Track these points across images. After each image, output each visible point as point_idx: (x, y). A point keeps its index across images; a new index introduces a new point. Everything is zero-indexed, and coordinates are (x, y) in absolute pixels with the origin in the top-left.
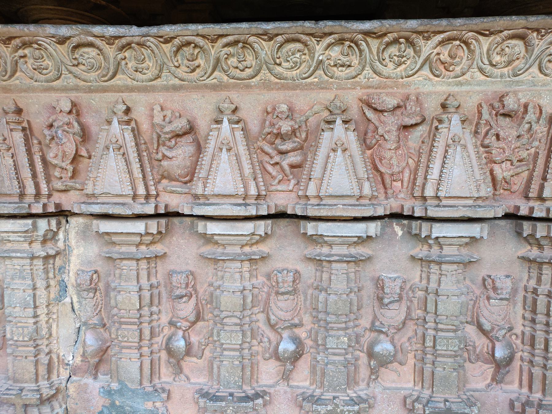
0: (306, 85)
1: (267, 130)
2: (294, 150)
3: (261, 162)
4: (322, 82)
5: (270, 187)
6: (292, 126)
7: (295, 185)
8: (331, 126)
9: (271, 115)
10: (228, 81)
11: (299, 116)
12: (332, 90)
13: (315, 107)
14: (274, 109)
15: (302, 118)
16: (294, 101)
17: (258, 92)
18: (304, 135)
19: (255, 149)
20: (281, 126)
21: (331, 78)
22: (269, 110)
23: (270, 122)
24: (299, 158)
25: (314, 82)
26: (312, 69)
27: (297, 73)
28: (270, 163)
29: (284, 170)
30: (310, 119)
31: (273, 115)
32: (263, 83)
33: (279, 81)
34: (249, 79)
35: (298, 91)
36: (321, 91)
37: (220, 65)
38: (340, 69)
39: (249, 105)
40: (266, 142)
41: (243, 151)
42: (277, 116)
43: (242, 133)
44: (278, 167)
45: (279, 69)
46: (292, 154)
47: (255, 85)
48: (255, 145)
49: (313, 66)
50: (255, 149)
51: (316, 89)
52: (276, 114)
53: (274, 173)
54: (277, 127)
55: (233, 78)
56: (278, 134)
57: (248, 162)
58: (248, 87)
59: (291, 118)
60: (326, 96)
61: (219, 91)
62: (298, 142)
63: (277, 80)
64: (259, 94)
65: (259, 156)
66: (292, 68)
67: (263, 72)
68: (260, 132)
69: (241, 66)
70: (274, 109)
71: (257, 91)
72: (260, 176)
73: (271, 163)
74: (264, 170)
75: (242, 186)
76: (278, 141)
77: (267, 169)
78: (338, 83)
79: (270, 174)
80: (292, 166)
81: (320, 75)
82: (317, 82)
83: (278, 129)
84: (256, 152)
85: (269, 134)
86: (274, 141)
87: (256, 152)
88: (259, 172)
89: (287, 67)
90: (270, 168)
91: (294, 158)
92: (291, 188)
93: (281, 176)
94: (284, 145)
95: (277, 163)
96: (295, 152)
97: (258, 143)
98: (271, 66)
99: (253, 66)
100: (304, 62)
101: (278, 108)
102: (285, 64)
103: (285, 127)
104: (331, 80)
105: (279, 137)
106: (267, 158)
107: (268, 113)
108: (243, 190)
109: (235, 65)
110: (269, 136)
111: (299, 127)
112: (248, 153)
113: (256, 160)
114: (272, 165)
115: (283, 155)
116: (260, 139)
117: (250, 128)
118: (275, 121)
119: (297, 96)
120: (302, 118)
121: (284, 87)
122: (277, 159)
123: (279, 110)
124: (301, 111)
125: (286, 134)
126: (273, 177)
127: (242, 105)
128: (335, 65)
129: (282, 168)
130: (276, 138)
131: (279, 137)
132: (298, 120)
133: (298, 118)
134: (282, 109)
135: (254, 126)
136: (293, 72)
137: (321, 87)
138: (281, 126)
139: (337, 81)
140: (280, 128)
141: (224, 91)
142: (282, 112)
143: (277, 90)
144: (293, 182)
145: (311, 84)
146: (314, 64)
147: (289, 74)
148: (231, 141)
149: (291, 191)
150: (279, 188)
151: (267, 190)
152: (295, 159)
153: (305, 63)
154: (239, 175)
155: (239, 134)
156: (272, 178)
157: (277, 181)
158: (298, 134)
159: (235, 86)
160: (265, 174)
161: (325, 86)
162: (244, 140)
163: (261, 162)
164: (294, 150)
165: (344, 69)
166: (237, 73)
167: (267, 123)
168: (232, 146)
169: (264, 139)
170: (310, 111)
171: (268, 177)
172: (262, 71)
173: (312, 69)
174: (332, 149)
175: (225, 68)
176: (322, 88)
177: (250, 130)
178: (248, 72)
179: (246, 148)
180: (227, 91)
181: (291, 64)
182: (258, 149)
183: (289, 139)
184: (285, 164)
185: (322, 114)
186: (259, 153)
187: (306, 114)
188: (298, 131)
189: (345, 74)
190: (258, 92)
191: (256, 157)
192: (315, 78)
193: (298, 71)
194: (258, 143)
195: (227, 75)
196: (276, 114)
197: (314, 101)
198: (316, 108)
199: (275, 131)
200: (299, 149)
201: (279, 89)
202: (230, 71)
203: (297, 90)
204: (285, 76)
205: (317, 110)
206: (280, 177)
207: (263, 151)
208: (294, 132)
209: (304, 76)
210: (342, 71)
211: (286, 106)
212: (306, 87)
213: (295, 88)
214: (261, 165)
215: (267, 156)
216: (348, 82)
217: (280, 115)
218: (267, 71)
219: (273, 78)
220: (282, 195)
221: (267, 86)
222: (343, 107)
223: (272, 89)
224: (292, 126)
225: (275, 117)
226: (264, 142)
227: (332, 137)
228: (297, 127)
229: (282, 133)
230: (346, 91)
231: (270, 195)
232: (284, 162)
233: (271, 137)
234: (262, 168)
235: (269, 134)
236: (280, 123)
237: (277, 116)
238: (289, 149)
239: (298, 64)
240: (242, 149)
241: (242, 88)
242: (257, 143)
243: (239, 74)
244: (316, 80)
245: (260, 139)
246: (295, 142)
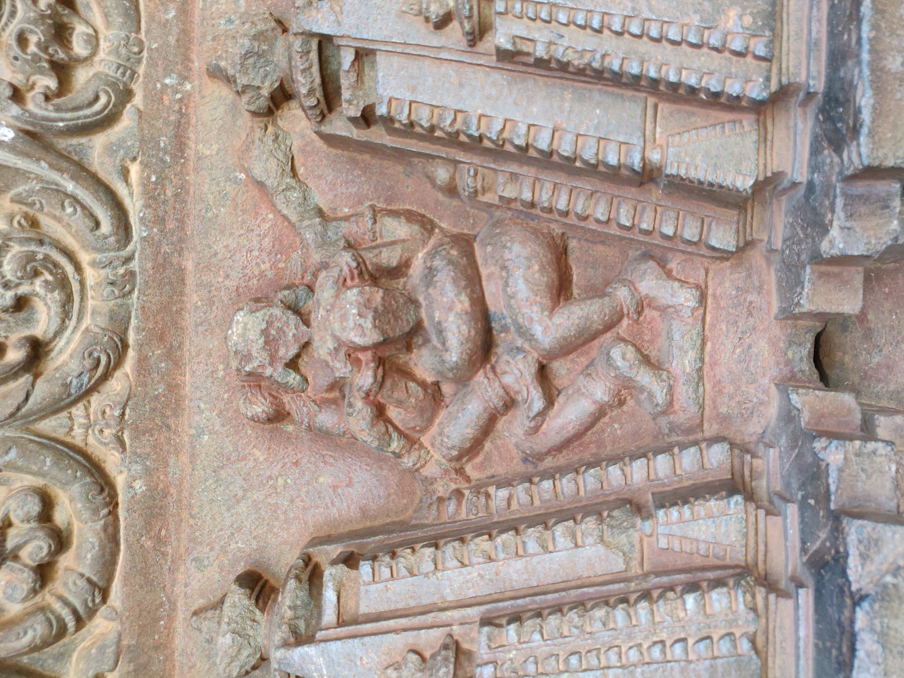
0: (160, 221)
1: (358, 421)
2: (472, 280)
3: (536, 466)
4: (147, 141)
5: (680, 418)
6: (342, 284)
7: (669, 274)
8: (347, 58)
9: (286, 398)
10: (116, 615)
11: (296, 256)
12: (189, 95)
13: (258, 171)
14: (255, 380)
15: (309, 236)
16: (231, 284)
17: (184, 458)
18: (398, 229)
19: (459, 493)
20: (340, 344)
21: (127, 95)
22: (260, 407)
23: (322, 404)
24: (517, 248)
25: (145, 183)
26: (70, 186)
27: (93, 264)
28: (542, 414)
29: (581, 332)
30: (319, 199)
31: (287, 388)
32: (138, 433)
33: (131, 353)
34: (112, 503)
35: (189, 265)
36: (190, 153)
37: (25, 660)
38: (79, 48)
39: (242, 508)
40: (424, 430)
41: (472, 573)
42: (293, 364)
43: (365, 568)
44: (560, 368)
45: (66, 358)
46: (491, 290)
47: (148, 472)
48: (441, 489)
49: (55, 176)
50: (459, 493)
51: (181, 174)
52: (277, 372)
53: (599, 390)
54: (341, 369)
55: (101, 590)
56: (381, 362)
57: (532, 546)
58: (154, 508)
59: (302, 292)
60: (216, 119)
61: (169, 658)
62: (432, 255)
63: (129, 365)
64: (193, 456)
65: (500, 470)
66: (63, 283)
67: (78, 431)
68: (378, 457)
69: (36, 548)
70: (255, 380)
71: (178, 464)
72: (614, 471)
73: (538, 404)
74: (581, 449)
75: (690, 600)
76: (423, 364)
77: (571, 430)
78: (152, 63)
79: (600, 413)
80: (561, 289)
81: (111, 150)
82: (145, 165)
83: (357, 363)
84: (479, 489)
85: (380, 412)
86: (423, 384)
87: (479, 489)
88: (590, 480)
89: (55, 309)
90: (570, 414)
91: (516, 279)
92: (685, 298)
93: (616, 353)
94: (440, 332)
95: (543, 373)
96: (484, 272)
97: (431, 470)
98: (43, 390)
99: (39, 482)
100: (34, 224)
101: (248, 357)
102: (43, 321)
103: (346, 319)
104: (138, 100)
105: (403, 358)
106: (513, 430)
107: (278, 416)
108: (718, 599)
109: (25, 580)
110: (393, 413)
111: (349, 246)
112: (483, 543)
113: (520, 491)
114: (550, 401)
115: (501, 338)
116: (408, 461)
117: (354, 512)
118: (319, 380)
119: (208, 267)
120: (309, 236)
121: (166, 330)
122: (515, 371)
123: (259, 358)
124: (281, 248)
125: (383, 315)
126: (624, 392)
127: (241, 551)
128: (62, 71)
129: (569, 347)
130: (408, 375)
131: (403, 358)
132: (316, 257)
133: (306, 257)
134: (254, 334)
135: (346, 490)
136: (90, 281)
137: (170, 151)
138: (340, 344)
139: (141, 70)
140: (352, 353)
141: (170, 630)
142: (270, 342)
143: (177, 364)
144: (649, 283)
145: (151, 196)
146: (42, 169)
147: (96, 303)
148: (410, 638)
149: (702, 299)
150: (683, 363)
151: (692, 436)
152: (519, 273)
153: (45, 221)
154: (619, 614)
155: (376, 587)
156: (622, 403)
157: (645, 377)
158: (390, 257)
159: (147, 577)
160: (600, 444)
161: (170, 131)
162: (406, 557)
163: (536, 466)
164: (472, 280)
165: (80, 30)
166: (76, 563)
167: (326, 419)
168: (436, 636)
169: (411, 441)
170: (279, 201)
171: (615, 429)
172: (78, 437)
173: (70, 186)
174: (473, 43)
175: (36, 630)
176: (180, 144)
177: (364, 511)
178: (70, 509)
179: (450, 549)
180: (171, 618)
181: (38, 286)
182: (460, 471)
183: (415, 303)
184: (549, 327)
185: (296, 144)
186: (481, 467)
187: (294, 218)
188: (369, 256)
189: (108, 24)
190: (184, 458)
191: (503, 493)
192: (125, 173)
193: (84, 258)
194: (431, 470)
195: (80, 622)
196: (277, 372)
197: (236, 181)
198: (267, 168)
199: (366, 378)
200: (470, 255)
201: (173, 357)
202: (57, 606)
203: (182, 270)
204: (102, 321)
205: (273, 164)
206: (622, 357)
207: (473, 448)
208: (375, 275)
209: (106, 227)
210: (94, 41)
211: (240, 317)
212: (171, 225)
213: (169, 279)
214: (549, 462)
215: (500, 425)
216: (151, 18)
217: (288, 352)
218: (78, 411)
219: (117, 385)
220: (725, 350)
221: (154, 418)
222: (261, 26)
223: (173, 388)
224: (342, 284)
225: (293, 378)
226: (425, 440)
227: (408, 52)
228: (346, 260)
229: (372, 337)
230: (197, 33)
231: (725, 419)
232: (538, 330)
233: (399, 403)
234: (562, 460)
235: (380, 412)
236: (323, 347)
237: (293, 364)
238: (463, 303)
239: (41, 252)
240: (459, 576)
241: (160, 541)
242: (429, 481)
243: (79, 558)
244: (135, 170)
245: (408, 461)
246: (430, 273)
